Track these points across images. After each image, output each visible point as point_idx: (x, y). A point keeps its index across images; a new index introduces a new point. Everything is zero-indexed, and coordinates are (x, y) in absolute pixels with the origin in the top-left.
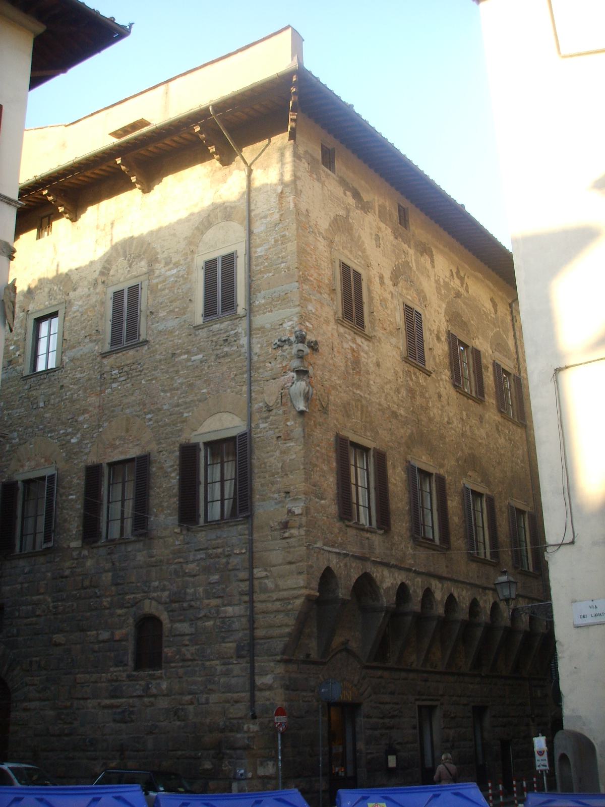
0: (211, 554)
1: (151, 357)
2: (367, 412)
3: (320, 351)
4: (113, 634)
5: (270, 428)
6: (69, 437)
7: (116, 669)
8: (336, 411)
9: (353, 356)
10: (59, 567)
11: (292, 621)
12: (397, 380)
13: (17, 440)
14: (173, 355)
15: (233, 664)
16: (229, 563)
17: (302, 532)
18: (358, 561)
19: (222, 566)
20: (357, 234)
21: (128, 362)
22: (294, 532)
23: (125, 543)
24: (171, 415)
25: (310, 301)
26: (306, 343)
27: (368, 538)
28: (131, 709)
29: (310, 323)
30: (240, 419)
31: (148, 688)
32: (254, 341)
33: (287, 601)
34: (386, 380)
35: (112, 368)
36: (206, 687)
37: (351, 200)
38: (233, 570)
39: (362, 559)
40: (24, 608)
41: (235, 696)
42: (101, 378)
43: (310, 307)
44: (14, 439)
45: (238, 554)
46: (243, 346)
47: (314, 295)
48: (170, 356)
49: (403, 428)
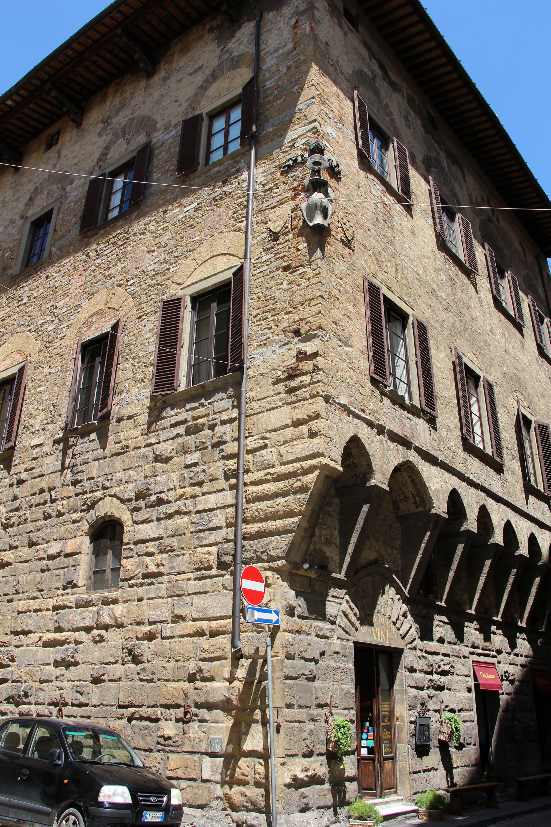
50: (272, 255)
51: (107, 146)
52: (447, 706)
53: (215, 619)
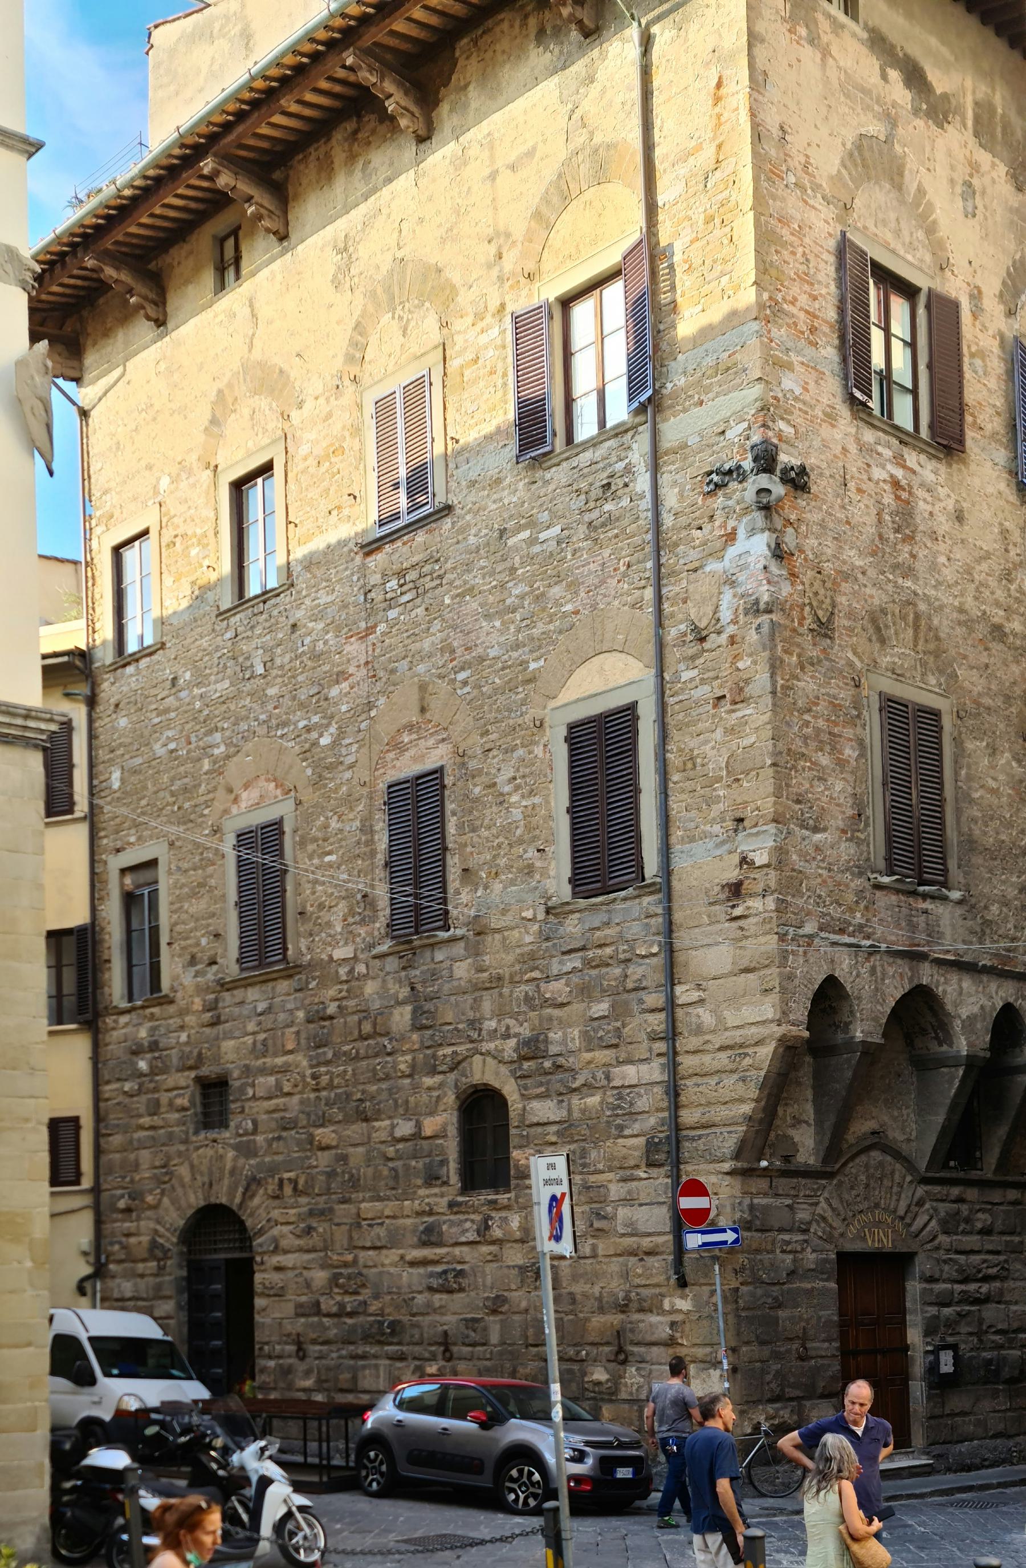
0: (593, 959)
1: (458, 542)
2: (930, 629)
3: (814, 489)
4: (419, 1125)
5: (702, 679)
6: (314, 735)
7: (427, 1192)
8: (851, 629)
9: (898, 498)
10: (316, 1000)
11: (754, 1093)
12: (1007, 550)
13: (222, 748)
14: (502, 532)
15: (641, 1179)
16: (626, 976)
17: (770, 903)
18: (899, 961)
19: (613, 983)
20: (915, 185)
21: (415, 559)
22: (755, 904)
23: (432, 945)
24: (503, 669)
25: (789, 366)
26: (778, 472)
27: (925, 912)
28: (459, 1267)
29: (788, 422)
30: (641, 665)
31: (487, 1228)
32: (665, 479)
33: (741, 1051)
34: (977, 554)
35: (384, 575)
36: (591, 1225)
37: (899, 93)
38: (635, 989)
39: (914, 956)
40: (261, 1080)
41: (646, 1243)
42: (365, 600)
43: (789, 383)
44: (217, 746)
45: (644, 957)
46: (642, 496)
47: (799, 353)
48: (496, 534)
49: (1018, 662)
50: (696, 671)
51: (358, 324)
52: (990, 1327)
53: (649, 1235)
